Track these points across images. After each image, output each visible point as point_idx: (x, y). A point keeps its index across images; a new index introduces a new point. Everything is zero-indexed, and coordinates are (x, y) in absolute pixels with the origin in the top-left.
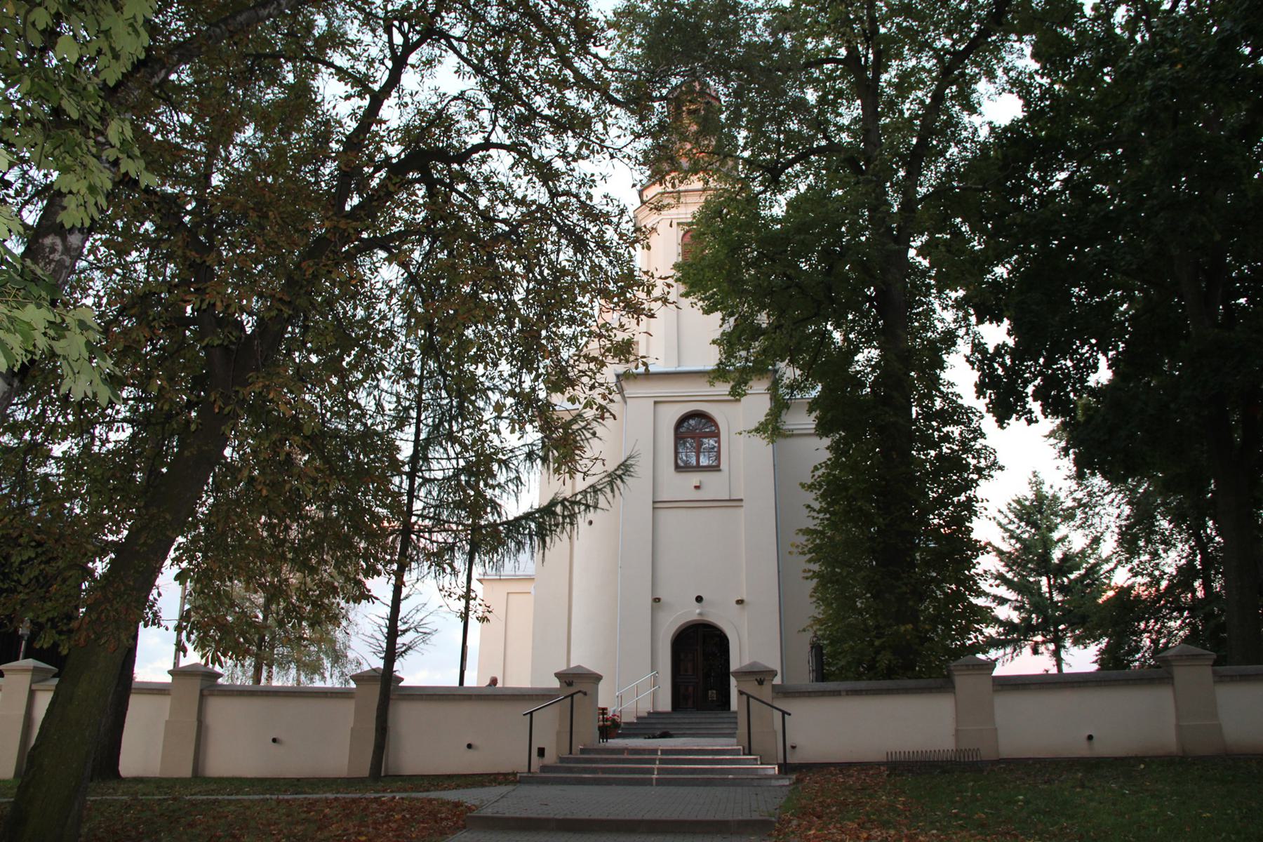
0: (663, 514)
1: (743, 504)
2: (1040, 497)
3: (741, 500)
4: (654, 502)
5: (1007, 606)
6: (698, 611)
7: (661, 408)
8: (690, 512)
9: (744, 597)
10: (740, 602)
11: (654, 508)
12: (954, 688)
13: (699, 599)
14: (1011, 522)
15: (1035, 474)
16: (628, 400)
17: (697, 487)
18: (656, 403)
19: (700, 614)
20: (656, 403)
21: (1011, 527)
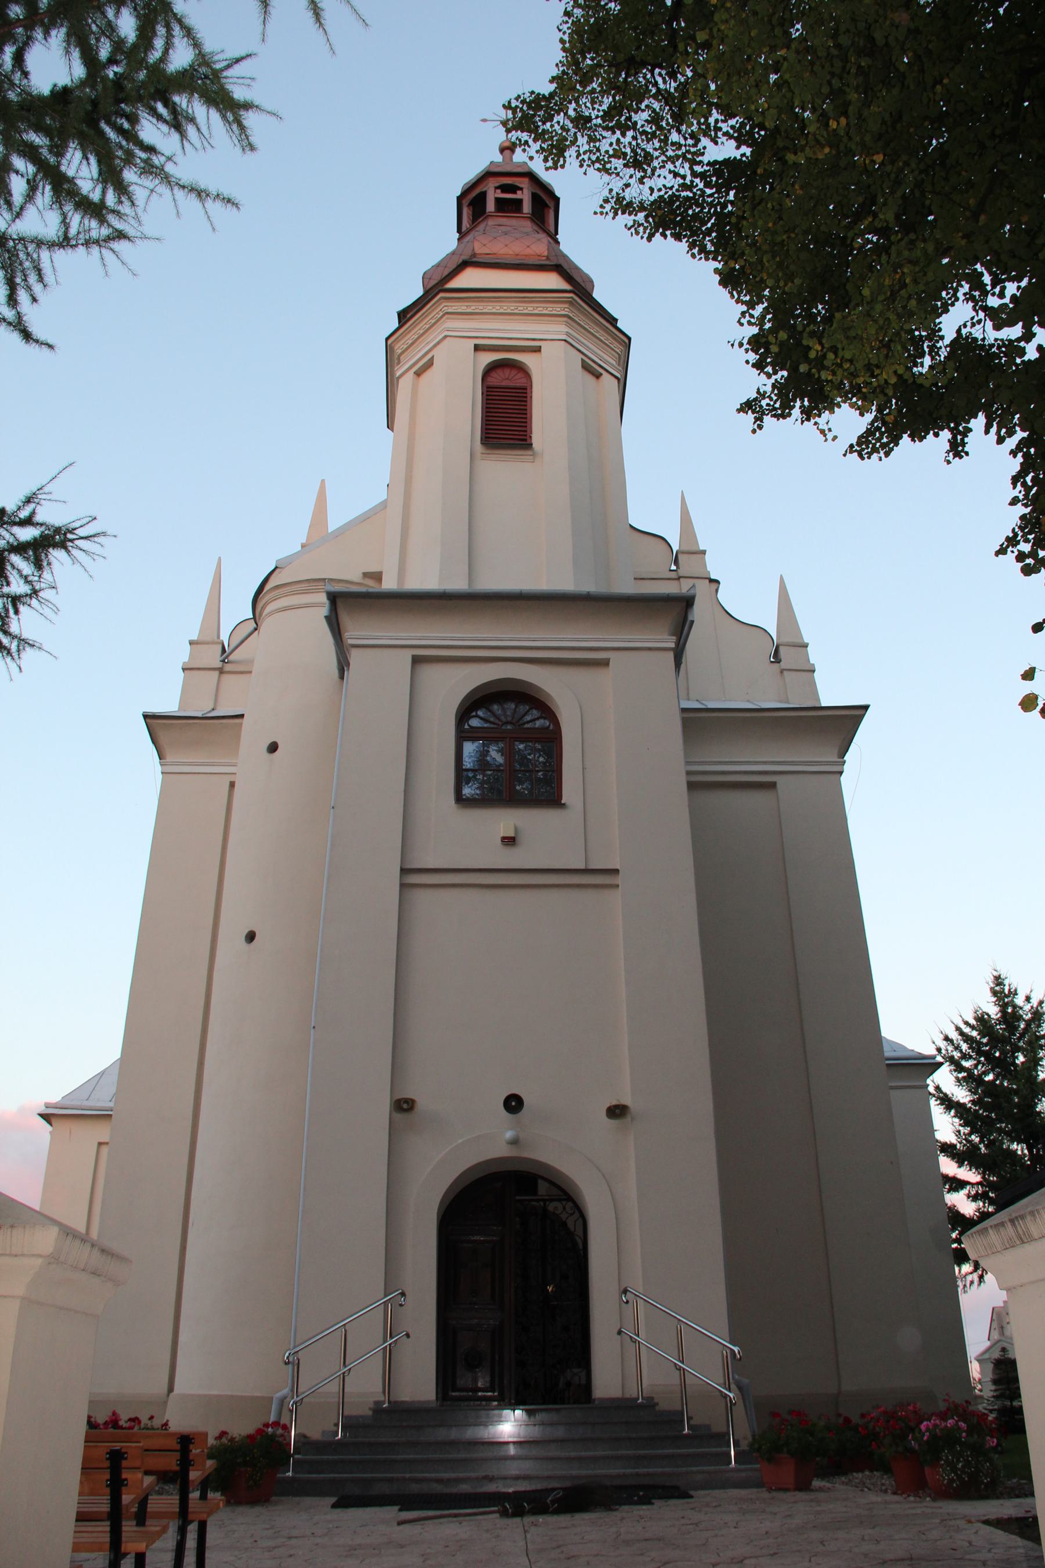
0: (425, 902)
1: (619, 880)
2: (1010, 1016)
3: (616, 871)
4: (404, 871)
5: (964, 1192)
6: (509, 1135)
7: (430, 673)
8: (490, 895)
9: (627, 1101)
10: (617, 1112)
11: (403, 886)
12: (90, 1402)
13: (513, 1104)
14: (965, 1056)
15: (998, 980)
16: (356, 657)
17: (509, 841)
18: (416, 661)
19: (515, 1142)
20: (477, 348)
21: (967, 1064)
